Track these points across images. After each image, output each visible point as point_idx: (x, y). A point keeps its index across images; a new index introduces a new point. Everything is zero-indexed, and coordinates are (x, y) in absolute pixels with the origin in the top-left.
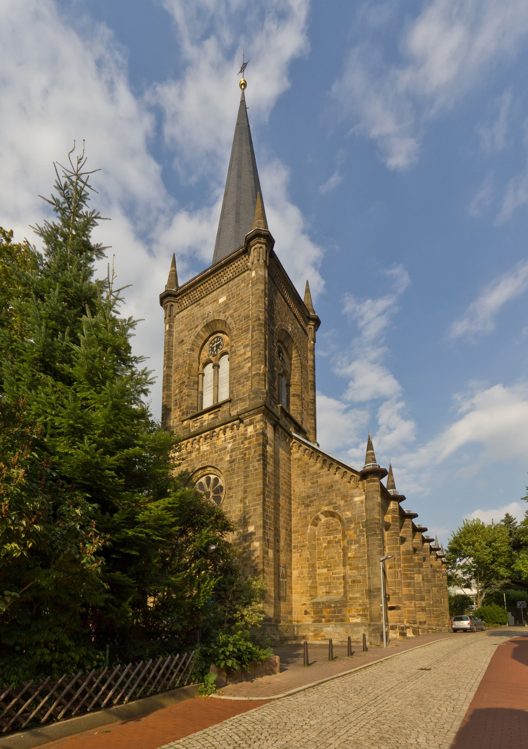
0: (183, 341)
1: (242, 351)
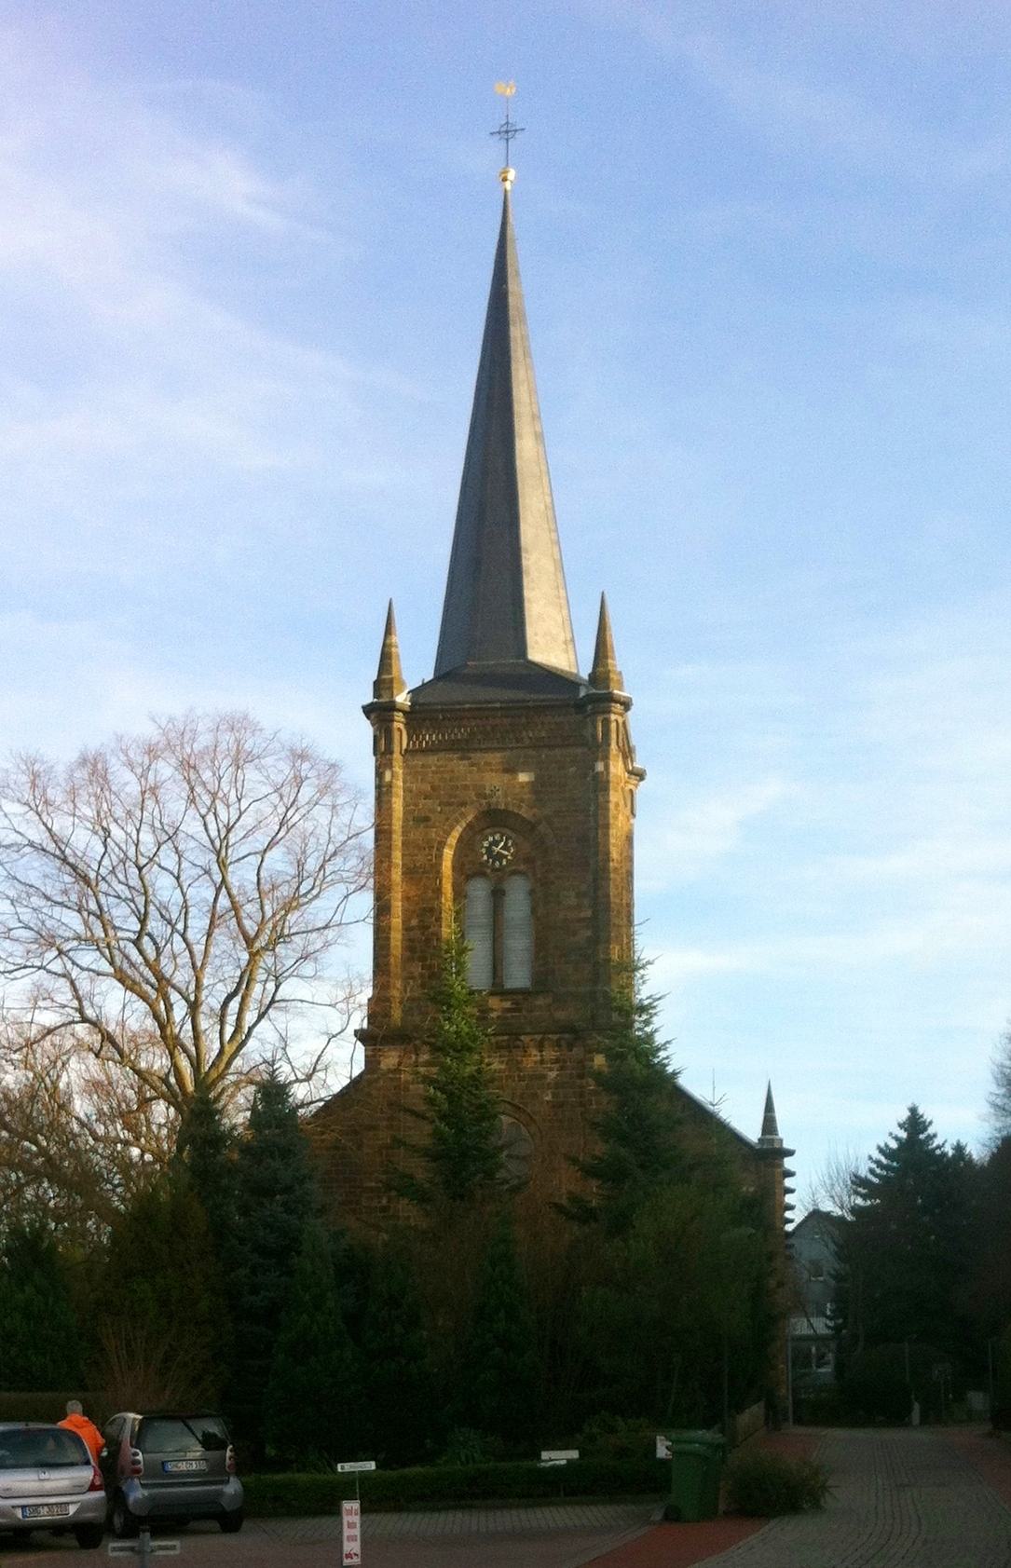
0: (427, 819)
1: (573, 901)
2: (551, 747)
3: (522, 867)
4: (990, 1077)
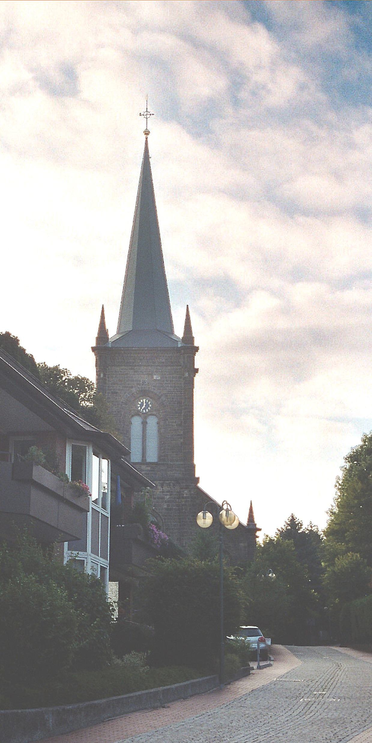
2: (166, 366)
3: (154, 413)
4: (334, 482)
